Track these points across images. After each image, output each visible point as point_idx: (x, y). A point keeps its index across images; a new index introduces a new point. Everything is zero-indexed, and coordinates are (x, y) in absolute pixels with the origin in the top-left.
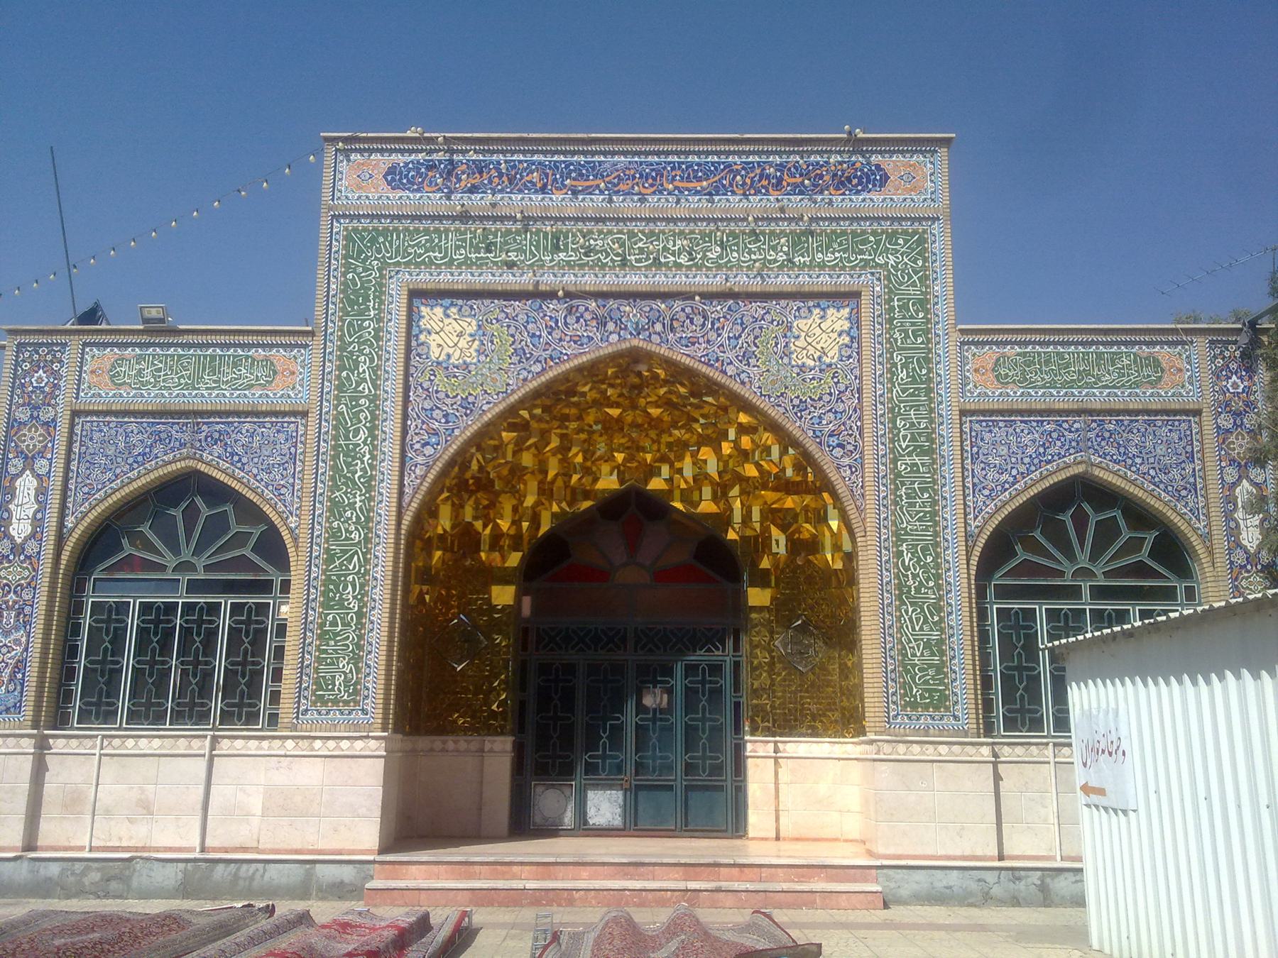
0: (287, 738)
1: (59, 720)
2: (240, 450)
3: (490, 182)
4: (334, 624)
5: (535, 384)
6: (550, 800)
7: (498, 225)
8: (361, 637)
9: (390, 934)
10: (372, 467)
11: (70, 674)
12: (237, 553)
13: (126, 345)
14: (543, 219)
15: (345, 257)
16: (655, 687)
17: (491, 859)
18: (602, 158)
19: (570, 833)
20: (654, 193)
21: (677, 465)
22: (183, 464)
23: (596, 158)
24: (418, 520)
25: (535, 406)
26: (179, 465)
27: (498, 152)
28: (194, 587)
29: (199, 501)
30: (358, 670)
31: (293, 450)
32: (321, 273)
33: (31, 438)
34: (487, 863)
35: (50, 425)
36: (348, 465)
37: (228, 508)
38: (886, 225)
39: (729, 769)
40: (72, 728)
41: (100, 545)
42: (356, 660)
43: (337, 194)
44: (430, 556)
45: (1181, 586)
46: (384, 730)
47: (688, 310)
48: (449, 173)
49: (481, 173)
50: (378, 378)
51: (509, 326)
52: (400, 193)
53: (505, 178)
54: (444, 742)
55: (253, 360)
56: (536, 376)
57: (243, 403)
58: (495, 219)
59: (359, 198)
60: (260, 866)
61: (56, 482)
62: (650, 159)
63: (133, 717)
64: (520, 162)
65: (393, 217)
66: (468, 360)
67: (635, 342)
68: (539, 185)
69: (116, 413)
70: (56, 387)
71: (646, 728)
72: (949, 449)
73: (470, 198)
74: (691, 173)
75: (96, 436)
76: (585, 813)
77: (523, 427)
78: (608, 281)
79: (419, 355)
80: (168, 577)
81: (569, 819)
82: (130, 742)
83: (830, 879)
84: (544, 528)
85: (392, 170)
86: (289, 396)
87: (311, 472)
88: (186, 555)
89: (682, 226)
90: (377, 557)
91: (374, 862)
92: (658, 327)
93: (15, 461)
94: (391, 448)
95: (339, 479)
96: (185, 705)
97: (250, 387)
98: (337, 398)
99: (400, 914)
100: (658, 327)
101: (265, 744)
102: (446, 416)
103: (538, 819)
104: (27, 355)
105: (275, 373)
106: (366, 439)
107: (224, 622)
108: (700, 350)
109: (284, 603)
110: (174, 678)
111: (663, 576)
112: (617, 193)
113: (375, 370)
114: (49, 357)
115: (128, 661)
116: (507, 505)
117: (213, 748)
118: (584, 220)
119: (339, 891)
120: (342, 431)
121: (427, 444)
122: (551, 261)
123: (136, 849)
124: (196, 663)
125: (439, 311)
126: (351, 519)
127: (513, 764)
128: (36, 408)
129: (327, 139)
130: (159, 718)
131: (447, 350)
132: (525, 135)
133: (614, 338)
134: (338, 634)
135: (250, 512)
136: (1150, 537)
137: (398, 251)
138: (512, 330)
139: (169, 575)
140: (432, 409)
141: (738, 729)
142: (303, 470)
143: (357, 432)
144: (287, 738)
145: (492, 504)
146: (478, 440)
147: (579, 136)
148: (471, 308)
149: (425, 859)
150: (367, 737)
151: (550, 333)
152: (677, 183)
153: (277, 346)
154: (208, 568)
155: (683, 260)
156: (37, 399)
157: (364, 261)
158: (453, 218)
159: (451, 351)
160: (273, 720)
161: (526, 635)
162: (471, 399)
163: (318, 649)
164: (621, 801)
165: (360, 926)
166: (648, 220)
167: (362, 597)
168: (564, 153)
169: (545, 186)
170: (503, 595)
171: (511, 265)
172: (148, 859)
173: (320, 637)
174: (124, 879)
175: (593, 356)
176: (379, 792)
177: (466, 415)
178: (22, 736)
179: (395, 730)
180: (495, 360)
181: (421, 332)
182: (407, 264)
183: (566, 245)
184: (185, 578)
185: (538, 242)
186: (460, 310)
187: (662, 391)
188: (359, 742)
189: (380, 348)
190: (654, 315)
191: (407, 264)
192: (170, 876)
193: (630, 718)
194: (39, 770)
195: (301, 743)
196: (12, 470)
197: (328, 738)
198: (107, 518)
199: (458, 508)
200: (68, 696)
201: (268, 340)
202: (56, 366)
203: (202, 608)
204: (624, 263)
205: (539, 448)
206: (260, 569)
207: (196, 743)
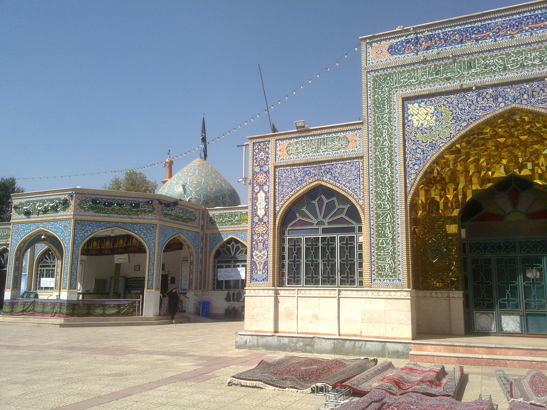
0: (368, 290)
1: (281, 284)
2: (337, 175)
3: (436, 43)
4: (382, 244)
5: (464, 131)
6: (482, 319)
7: (441, 62)
8: (394, 249)
9: (433, 374)
10: (392, 177)
11: (283, 266)
12: (339, 217)
13: (291, 138)
14: (462, 55)
15: (373, 89)
16: (532, 268)
17: (464, 344)
18: (490, 22)
19: (495, 334)
20: (518, 33)
21: (536, 162)
22: (316, 183)
23: (487, 22)
24: (413, 199)
25: (463, 142)
26: (315, 183)
27: (438, 29)
28: (325, 231)
29: (323, 197)
30: (395, 263)
31: (358, 173)
32: (364, 97)
33: (261, 178)
34: (462, 346)
35: (267, 172)
36: (382, 177)
37: (334, 199)
40: (286, 287)
41: (288, 216)
42: (393, 258)
43: (368, 62)
46: (409, 288)
47: (541, 86)
48: (416, 43)
49: (431, 40)
50: (392, 138)
51: (449, 107)
52: (395, 56)
53: (442, 40)
54: (431, 293)
55: (340, 138)
56: (464, 128)
57: (337, 156)
58: (439, 60)
59: (378, 62)
60: (364, 343)
61: (271, 194)
62: (514, 17)
63: (307, 282)
64: (449, 31)
66: (431, 125)
67: (514, 105)
68: (459, 40)
69: (290, 165)
70: (268, 157)
71: (529, 288)
73: (427, 52)
75: (284, 175)
76: (501, 326)
77: (458, 151)
78: (498, 78)
79: (409, 126)
80: (314, 228)
81: (494, 328)
82: (308, 292)
83: (531, 355)
84: (469, 197)
85: (391, 47)
86: (355, 151)
87: (367, 182)
88: (320, 218)
89: (534, 46)
90: (398, 215)
91: (411, 343)
92: (525, 96)
93: (257, 187)
94: (399, 168)
95: (379, 183)
96: (326, 277)
97: (339, 149)
98: (375, 149)
99: (429, 367)
100: (525, 96)
101: (360, 293)
102: (423, 151)
103: (478, 328)
104: (257, 146)
105: (349, 142)
106: (388, 165)
107: (338, 244)
109: (360, 236)
110: (321, 267)
111: (532, 216)
112: (498, 36)
113: (390, 135)
114: (264, 147)
115: (303, 261)
116: (451, 187)
117: (339, 295)
118: (482, 52)
119: (397, 354)
120: (378, 163)
121: (416, 164)
122: (468, 74)
123: (314, 334)
124: (329, 261)
126: (385, 199)
127: (463, 303)
128: (262, 166)
129: (361, 39)
130: (317, 283)
131: (421, 122)
132: (451, 19)
133: (502, 105)
134: (384, 248)
135: (344, 199)
137: (396, 82)
138: (451, 108)
139: (315, 227)
140: (416, 149)
142: (363, 181)
143: (384, 162)
144: (368, 290)
145: (444, 189)
146: (436, 162)
147: (477, 13)
148: (431, 101)
149: (433, 343)
150: (402, 291)
151: (470, 107)
152: (530, 26)
153: (349, 130)
155: (536, 62)
156: (262, 163)
157: (382, 89)
158: (420, 63)
159: (423, 122)
160: (361, 283)
161: (463, 247)
162: (434, 142)
163: (377, 254)
164: (519, 320)
165: (416, 370)
166: (516, 46)
167: (393, 232)
168: (470, 23)
169: (462, 40)
170: (452, 229)
171: (448, 79)
172: (320, 338)
173: (377, 249)
174: (312, 346)
175: (492, 115)
176: (409, 314)
177: (432, 150)
178: (269, 289)
179: (413, 288)
180: (444, 123)
181: (409, 116)
182: (400, 87)
183: (475, 66)
184: (321, 228)
185: (461, 66)
186: (426, 103)
187: (527, 127)
188: (398, 293)
189: (391, 125)
190: (522, 91)
191: (400, 87)
192: (328, 345)
193: (520, 283)
194: (277, 302)
195: (374, 292)
196: (256, 191)
197: (385, 291)
198: (290, 206)
199: (427, 192)
200: (283, 274)
201: (345, 128)
203: (328, 239)
204: (505, 69)
205: (465, 160)
206: (349, 223)
207: (332, 292)
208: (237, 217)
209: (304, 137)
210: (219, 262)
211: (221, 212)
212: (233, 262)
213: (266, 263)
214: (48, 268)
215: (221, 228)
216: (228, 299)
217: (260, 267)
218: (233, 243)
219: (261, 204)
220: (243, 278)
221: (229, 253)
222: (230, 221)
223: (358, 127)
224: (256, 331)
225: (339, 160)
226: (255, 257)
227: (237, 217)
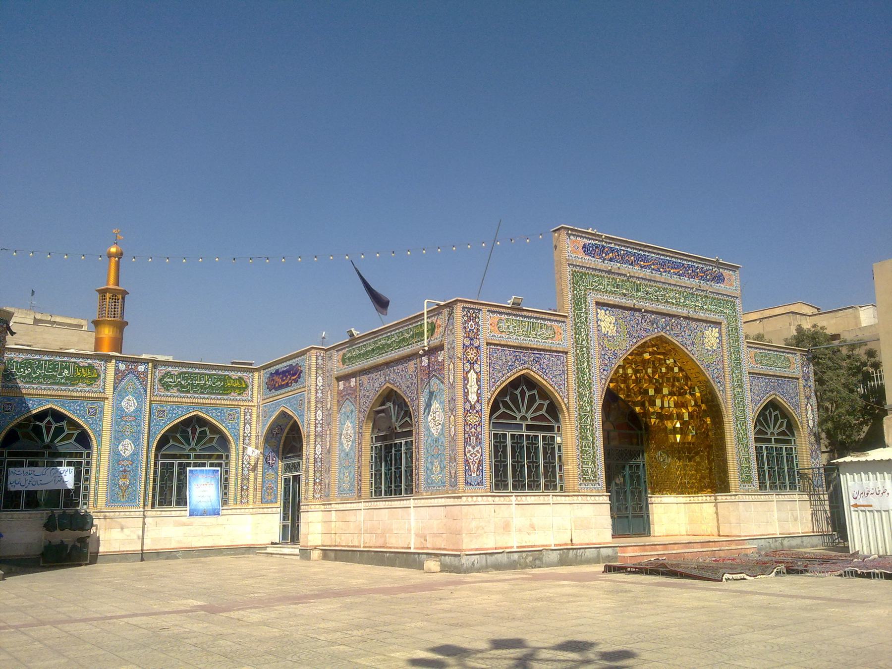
28: (529, 427)
37: (535, 392)
42: (594, 462)
44: (706, 423)
45: (85, 452)
65: (587, 268)
72: (747, 386)
74: (675, 266)
83: (737, 545)
97: (547, 338)
113: (587, 335)
141: (646, 493)
154: (532, 419)
156: (472, 335)
158: (606, 272)
167: (593, 435)
174: (540, 559)
184: (524, 424)
201: (552, 318)
208: (66, 371)
211: (29, 356)
212: (46, 455)
213: (480, 463)
214: (185, 461)
215: (26, 388)
216: (49, 526)
218: (49, 418)
219: (473, 388)
220: (70, 485)
221: (47, 436)
222: (50, 377)
224: (477, 549)
226: (468, 455)
227: (66, 371)
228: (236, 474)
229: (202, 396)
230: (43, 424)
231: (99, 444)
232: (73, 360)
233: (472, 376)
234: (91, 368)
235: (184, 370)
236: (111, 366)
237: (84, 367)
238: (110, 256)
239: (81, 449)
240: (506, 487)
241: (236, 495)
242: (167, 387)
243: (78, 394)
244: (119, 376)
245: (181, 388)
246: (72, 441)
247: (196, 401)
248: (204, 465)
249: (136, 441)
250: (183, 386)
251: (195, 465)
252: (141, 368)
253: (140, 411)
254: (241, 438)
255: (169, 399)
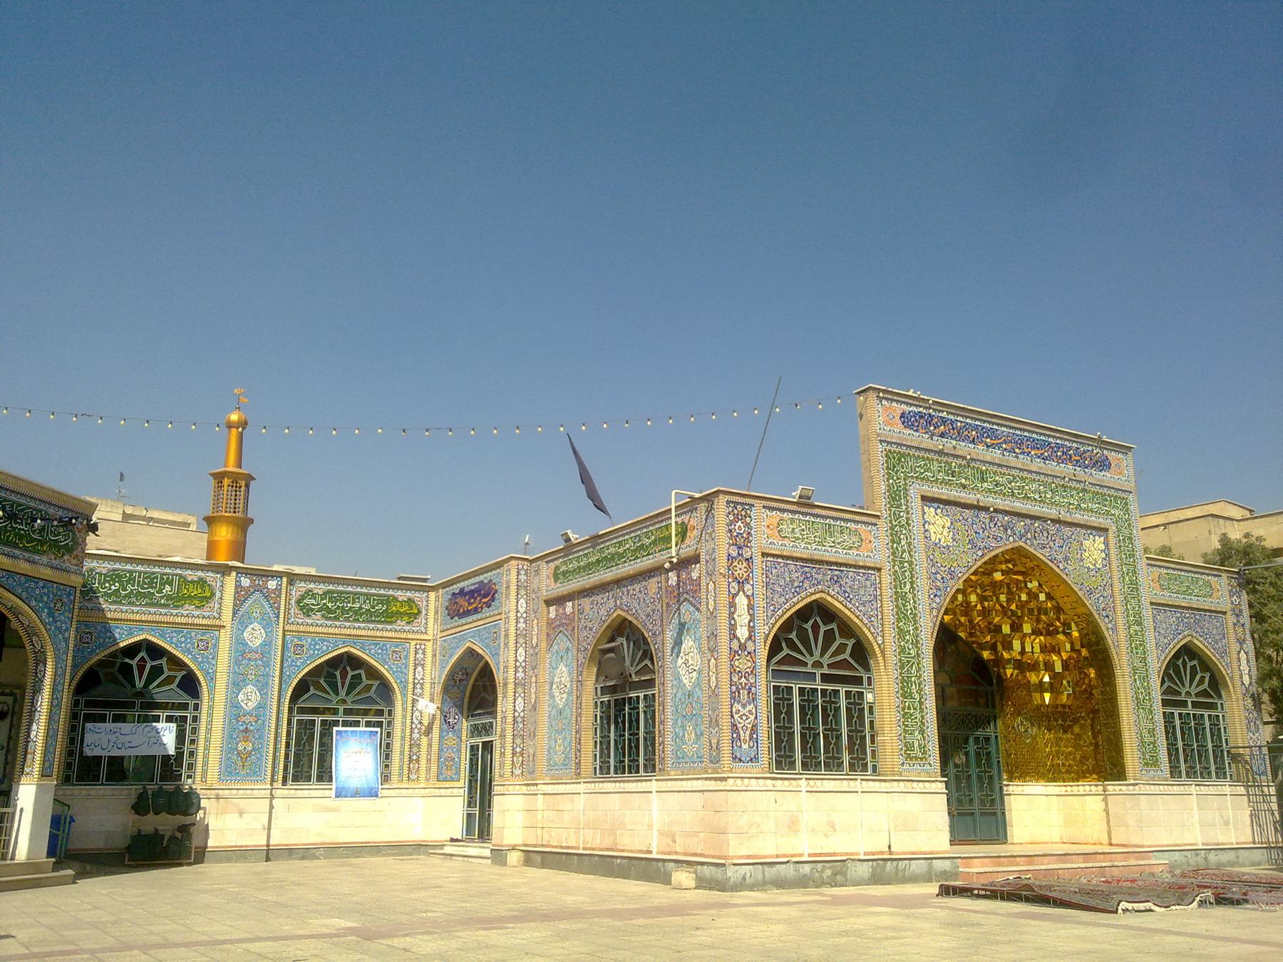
28: (826, 678)
37: (834, 626)
38: (1112, 492)
39: (998, 802)
42: (922, 732)
45: (192, 703)
65: (908, 446)
74: (1036, 445)
75: (774, 571)
83: (1137, 859)
108: (1046, 552)
113: (909, 544)
123: (847, 854)
125: (932, 510)
136: (851, 643)
139: (1182, 698)
154: (830, 666)
156: (740, 541)
158: (936, 452)
174: (844, 874)
184: (818, 672)
192: (864, 870)
202: (748, 520)
208: (168, 588)
209: (803, 514)
210: (89, 704)
211: (117, 566)
213: (754, 729)
215: (111, 610)
217: (745, 735)
218: (143, 654)
219: (742, 618)
222: (144, 596)
223: (874, 520)
224: (749, 857)
225: (851, 566)
226: (736, 717)
227: (168, 588)
228: (403, 738)
229: (356, 625)
230: (134, 663)
231: (212, 691)
232: (179, 571)
233: (742, 601)
234: (202, 582)
235: (331, 587)
236: (230, 581)
237: (193, 582)
238: (230, 426)
239: (185, 698)
240: (792, 765)
241: (401, 768)
242: (307, 610)
243: (184, 620)
244: (241, 596)
245: (328, 613)
246: (174, 686)
247: (348, 632)
248: (357, 724)
249: (263, 688)
250: (330, 611)
251: (345, 724)
252: (272, 584)
253: (270, 644)
254: (410, 686)
255: (312, 629)
